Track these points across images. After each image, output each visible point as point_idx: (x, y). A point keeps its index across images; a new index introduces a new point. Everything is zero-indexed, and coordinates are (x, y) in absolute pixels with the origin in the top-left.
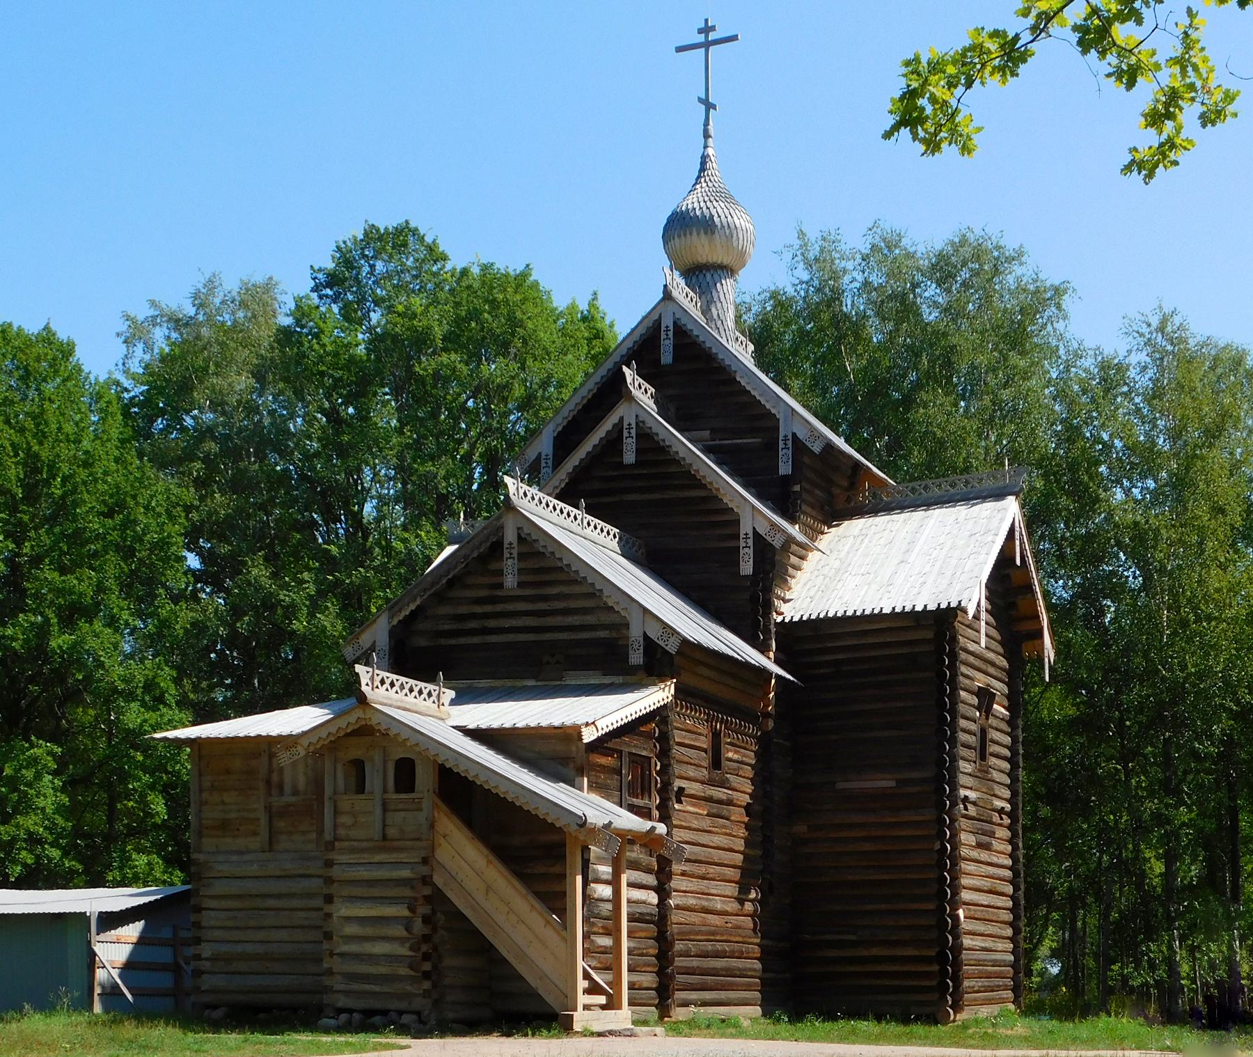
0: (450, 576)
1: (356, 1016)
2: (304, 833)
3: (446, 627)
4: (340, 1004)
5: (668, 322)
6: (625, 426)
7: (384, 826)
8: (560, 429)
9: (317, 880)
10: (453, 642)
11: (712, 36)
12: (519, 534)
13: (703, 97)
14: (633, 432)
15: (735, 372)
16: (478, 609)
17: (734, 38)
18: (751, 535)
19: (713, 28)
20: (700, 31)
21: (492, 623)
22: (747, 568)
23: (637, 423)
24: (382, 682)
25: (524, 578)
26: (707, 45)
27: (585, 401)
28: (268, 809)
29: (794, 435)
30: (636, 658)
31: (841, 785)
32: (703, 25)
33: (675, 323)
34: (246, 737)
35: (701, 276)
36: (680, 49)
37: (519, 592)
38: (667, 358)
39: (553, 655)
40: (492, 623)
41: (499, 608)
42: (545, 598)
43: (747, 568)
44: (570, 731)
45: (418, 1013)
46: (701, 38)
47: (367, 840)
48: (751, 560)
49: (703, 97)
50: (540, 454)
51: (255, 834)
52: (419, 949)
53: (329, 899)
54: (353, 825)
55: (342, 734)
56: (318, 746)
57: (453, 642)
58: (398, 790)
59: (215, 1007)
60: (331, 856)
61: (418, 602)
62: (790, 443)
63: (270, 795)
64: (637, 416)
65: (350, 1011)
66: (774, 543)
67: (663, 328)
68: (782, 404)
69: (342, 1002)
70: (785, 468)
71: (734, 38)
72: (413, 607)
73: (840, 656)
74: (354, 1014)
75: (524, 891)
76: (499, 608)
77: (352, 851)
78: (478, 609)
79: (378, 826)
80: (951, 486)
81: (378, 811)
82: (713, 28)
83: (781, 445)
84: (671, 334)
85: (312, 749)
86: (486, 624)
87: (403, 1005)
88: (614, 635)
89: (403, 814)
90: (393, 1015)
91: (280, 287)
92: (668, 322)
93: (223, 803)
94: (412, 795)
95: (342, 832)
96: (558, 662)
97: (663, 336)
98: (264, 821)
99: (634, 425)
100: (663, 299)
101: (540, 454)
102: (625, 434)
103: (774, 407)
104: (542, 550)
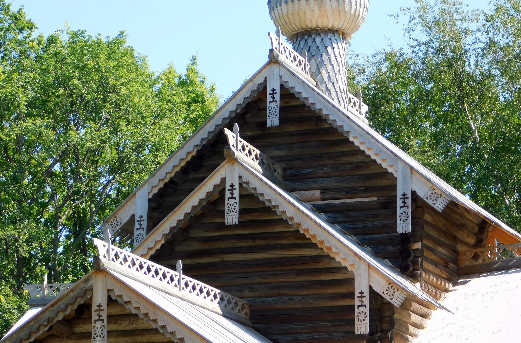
5: (274, 85)
6: (228, 187)
8: (156, 191)
15: (348, 132)
23: (240, 185)
27: (183, 164)
29: (414, 193)
33: (282, 86)
35: (310, 41)
48: (368, 319)
50: (133, 216)
62: (409, 202)
64: (240, 177)
66: (392, 302)
67: (269, 91)
68: (400, 164)
83: (400, 203)
92: (274, 85)
97: (269, 98)
99: (237, 186)
100: (269, 63)
101: (133, 216)
102: (228, 195)
103: (391, 166)
104: (134, 312)
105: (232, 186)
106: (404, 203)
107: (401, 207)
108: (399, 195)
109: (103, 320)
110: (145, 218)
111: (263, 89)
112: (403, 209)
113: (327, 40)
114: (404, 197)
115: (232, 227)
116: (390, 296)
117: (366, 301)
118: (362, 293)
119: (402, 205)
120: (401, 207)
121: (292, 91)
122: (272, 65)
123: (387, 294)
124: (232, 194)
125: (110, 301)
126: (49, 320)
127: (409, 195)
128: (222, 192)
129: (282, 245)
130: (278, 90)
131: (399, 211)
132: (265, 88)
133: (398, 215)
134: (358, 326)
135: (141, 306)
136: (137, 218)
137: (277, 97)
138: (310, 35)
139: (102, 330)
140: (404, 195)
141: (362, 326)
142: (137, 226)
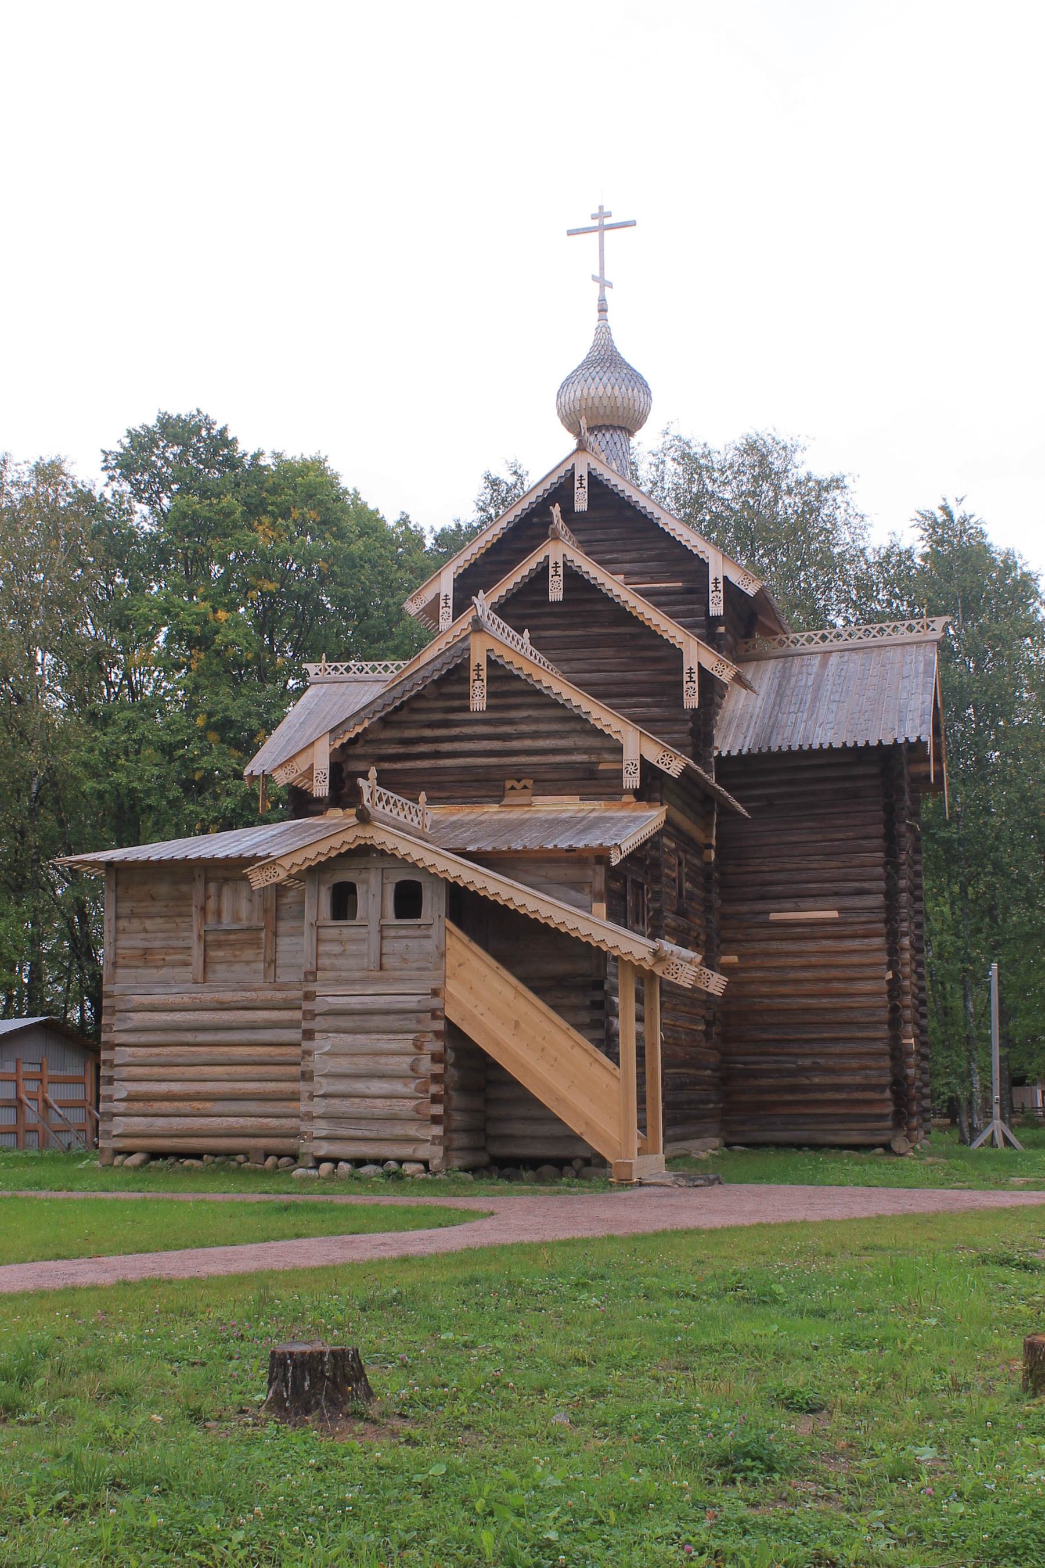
0: (405, 699)
1: (345, 1167)
2: (248, 963)
3: (391, 751)
4: (321, 1153)
5: (581, 471)
6: (551, 565)
7: (381, 954)
8: (461, 571)
9: (122, 1008)
10: (398, 766)
11: (607, 221)
12: (488, 656)
13: (598, 274)
14: (560, 571)
16: (428, 733)
17: (631, 224)
18: (696, 670)
19: (609, 215)
20: (594, 217)
21: (446, 747)
22: (691, 701)
23: (564, 564)
24: (380, 799)
25: (494, 702)
26: (603, 228)
27: (489, 545)
28: (203, 938)
29: (725, 578)
30: (632, 780)
31: (774, 916)
32: (596, 211)
33: (589, 473)
34: (136, 862)
35: (600, 436)
36: (570, 233)
37: (488, 716)
38: (581, 504)
39: (519, 781)
40: (446, 747)
41: (455, 731)
42: (511, 722)
43: (691, 701)
44: (585, 855)
45: (426, 1163)
46: (596, 223)
47: (359, 970)
49: (598, 274)
50: (438, 595)
51: (187, 964)
52: (427, 1091)
53: (309, 1035)
54: (341, 954)
55: (333, 854)
56: (303, 868)
57: (398, 766)
58: (399, 915)
59: (130, 1153)
60: (311, 987)
61: (366, 724)
62: (721, 586)
63: (206, 923)
64: (564, 555)
65: (335, 1161)
67: (576, 477)
69: (324, 1149)
70: (716, 608)
71: (631, 224)
72: (359, 729)
73: (774, 791)
74: (341, 1164)
75: (565, 1025)
76: (455, 731)
77: (339, 982)
78: (428, 733)
79: (374, 956)
80: (827, 637)
81: (375, 937)
82: (609, 215)
83: (712, 587)
84: (585, 483)
85: (294, 871)
86: (438, 749)
87: (406, 1151)
88: (594, 758)
89: (405, 942)
90: (393, 1166)
91: (69, 460)
92: (581, 471)
93: (146, 931)
94: (418, 921)
95: (325, 961)
96: (525, 787)
97: (577, 484)
98: (197, 951)
99: (561, 564)
100: (577, 450)
101: (438, 595)
102: (551, 572)
104: (516, 672)
105: (556, 563)
106: (716, 587)
108: (711, 580)
109: (482, 680)
110: (451, 596)
111: (570, 475)
113: (615, 436)
115: (556, 603)
117: (695, 677)
118: (691, 669)
121: (600, 478)
122: (580, 453)
124: (556, 571)
125: (491, 663)
126: (424, 678)
127: (721, 580)
128: (546, 569)
129: (558, 629)
130: (586, 477)
131: (711, 596)
132: (573, 474)
135: (908, 634)
136: (442, 597)
138: (600, 431)
140: (716, 579)
142: (442, 604)
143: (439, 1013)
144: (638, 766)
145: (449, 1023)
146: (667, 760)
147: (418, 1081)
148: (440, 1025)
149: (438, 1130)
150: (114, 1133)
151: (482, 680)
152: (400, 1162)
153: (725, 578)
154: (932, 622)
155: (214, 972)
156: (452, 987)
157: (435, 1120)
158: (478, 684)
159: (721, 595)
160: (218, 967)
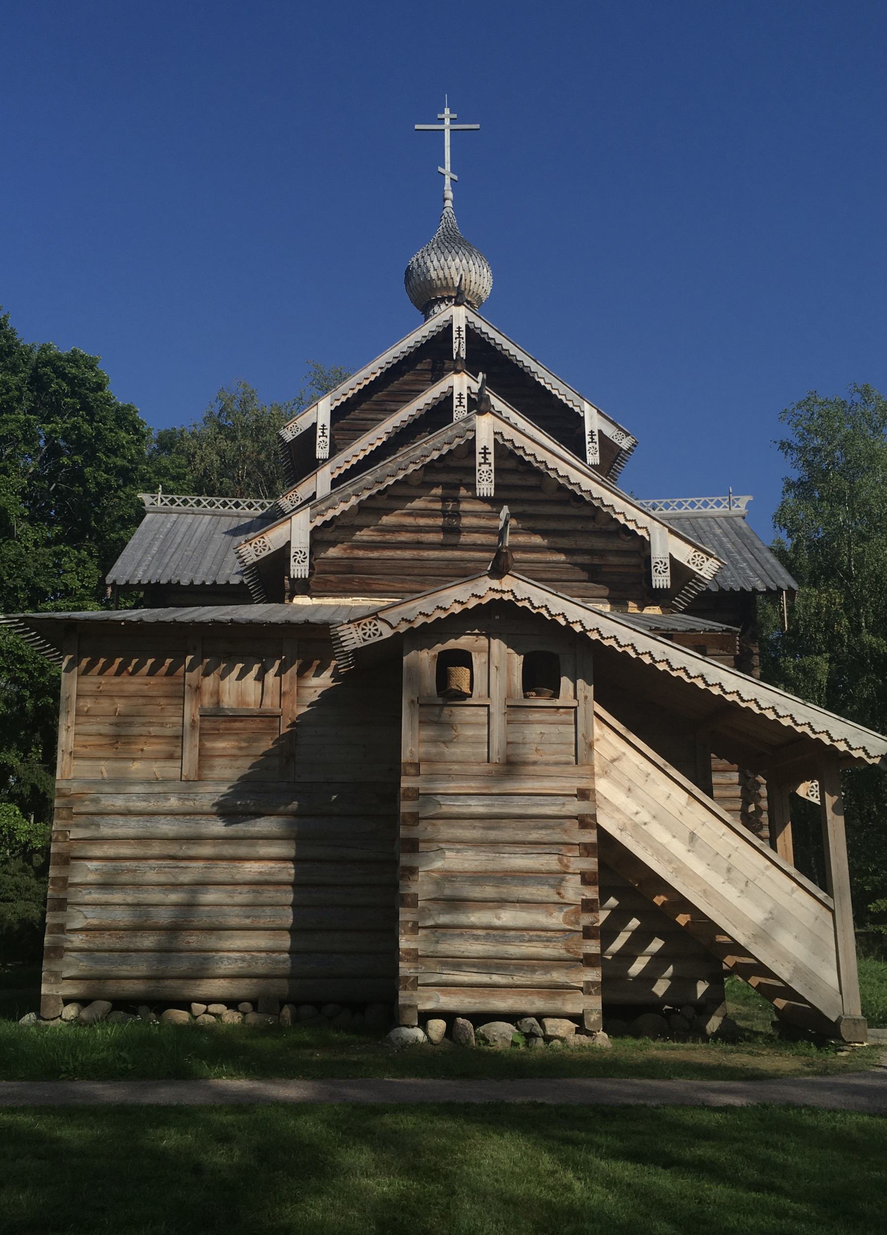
4: (429, 1006)
6: (455, 395)
10: (375, 554)
12: (495, 440)
29: (600, 432)
45: (577, 1019)
50: (315, 425)
52: (577, 923)
57: (375, 554)
62: (596, 438)
64: (469, 388)
67: (455, 328)
83: (588, 439)
101: (315, 425)
107: (589, 443)
108: (587, 432)
110: (328, 426)
112: (591, 445)
114: (485, 451)
116: (693, 559)
118: (485, 448)
119: (590, 440)
120: (589, 443)
123: (701, 565)
124: (460, 402)
127: (596, 433)
131: (588, 446)
132: (451, 326)
133: (587, 449)
134: (656, 578)
136: (319, 426)
137: (491, 458)
139: (481, 478)
141: (660, 578)
143: (590, 820)
144: (668, 565)
145: (602, 833)
146: (698, 560)
147: (566, 910)
148: (591, 837)
149: (594, 975)
150: (65, 975)
151: (490, 464)
152: (540, 1017)
153: (600, 432)
154: (738, 499)
155: (212, 768)
156: (602, 786)
157: (589, 961)
158: (485, 468)
159: (597, 446)
160: (218, 762)
